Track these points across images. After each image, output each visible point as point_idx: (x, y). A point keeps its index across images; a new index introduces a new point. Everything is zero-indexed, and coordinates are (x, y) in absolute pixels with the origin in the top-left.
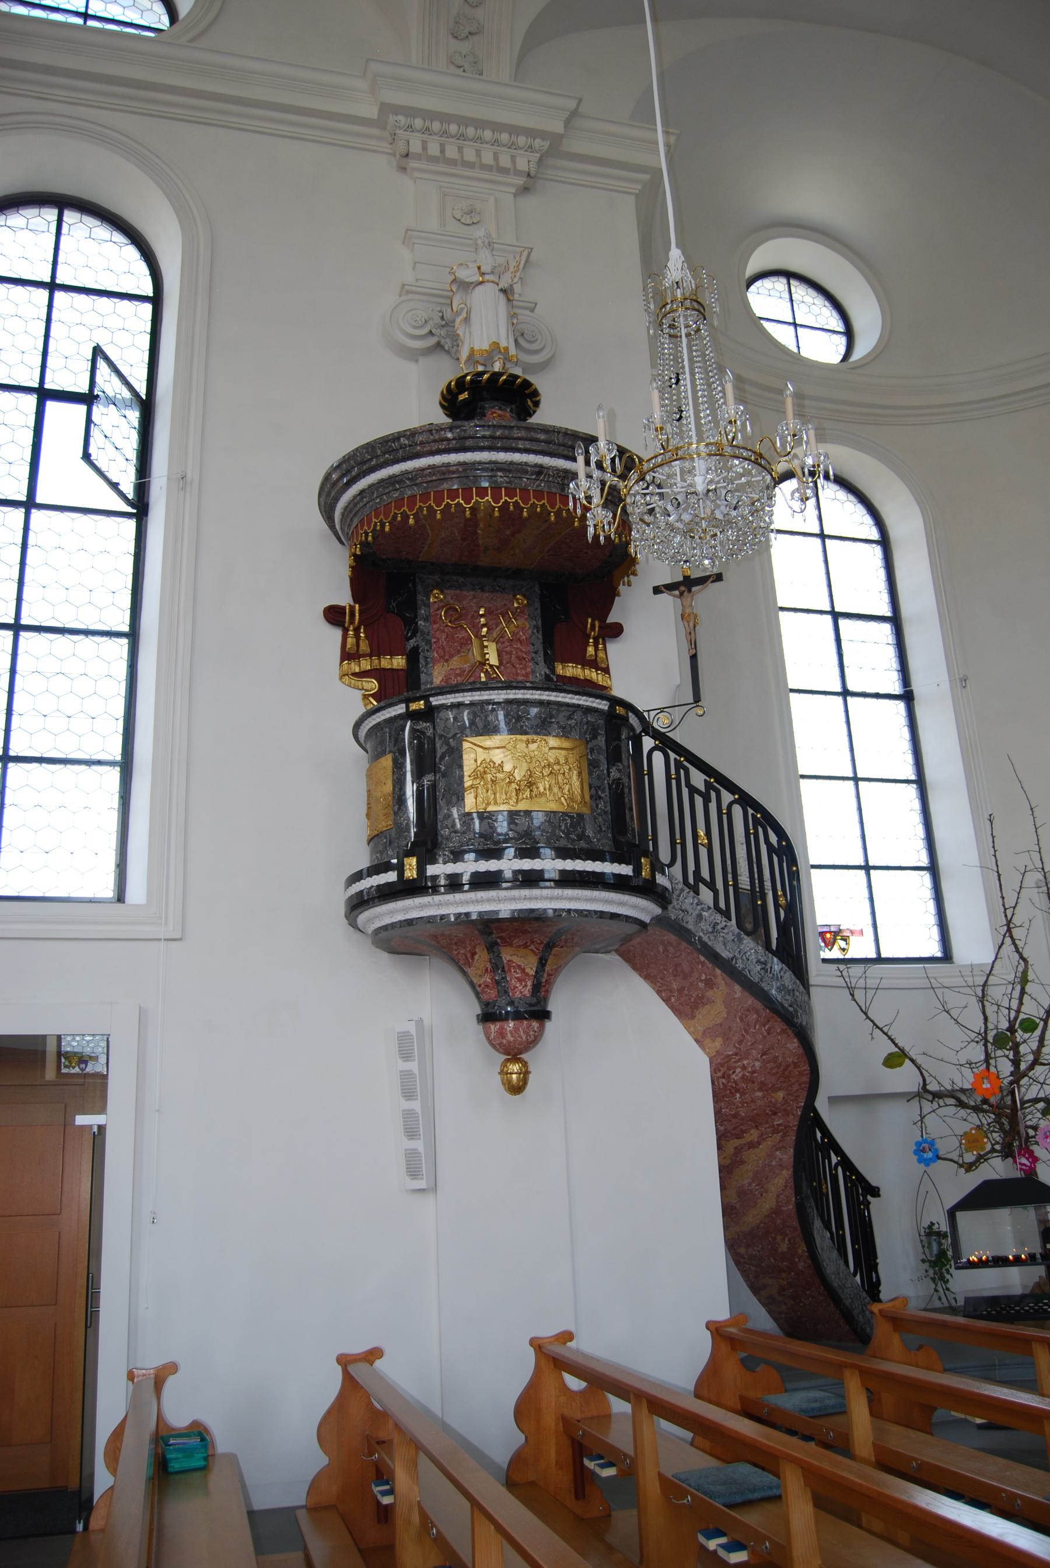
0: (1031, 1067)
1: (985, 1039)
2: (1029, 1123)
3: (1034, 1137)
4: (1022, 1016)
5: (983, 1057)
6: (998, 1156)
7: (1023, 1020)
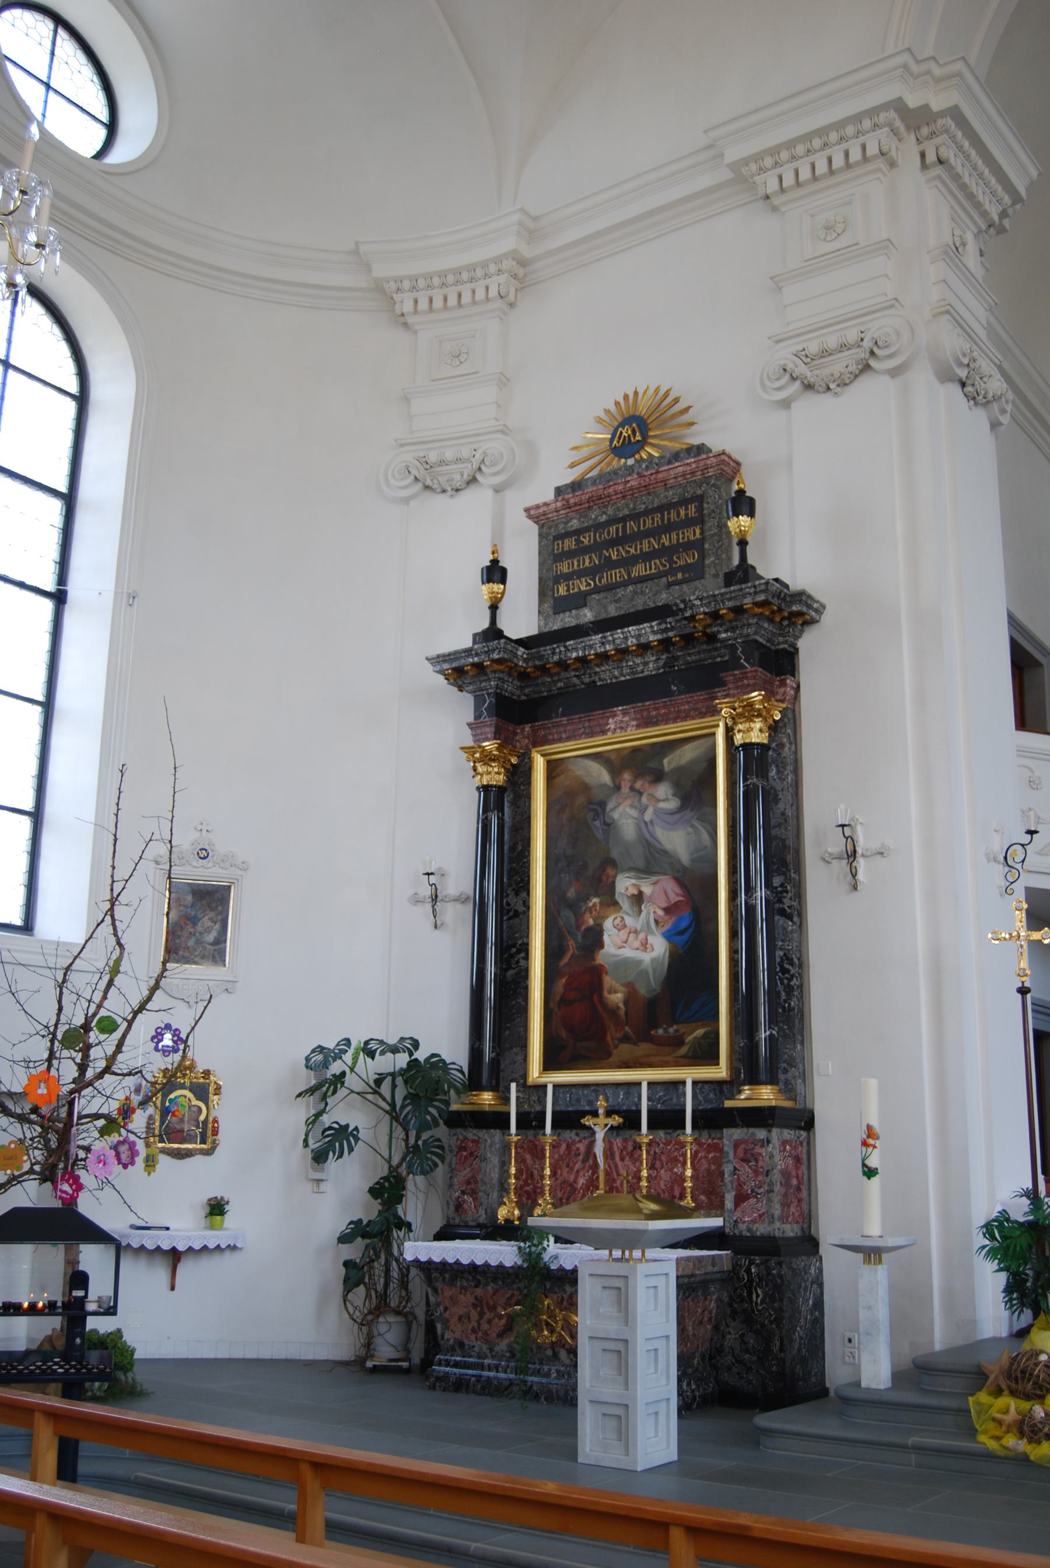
0: (100, 1076)
1: (54, 1034)
2: (81, 1143)
3: (84, 1160)
4: (103, 1013)
5: (46, 1055)
6: (35, 1179)
7: (102, 1019)
